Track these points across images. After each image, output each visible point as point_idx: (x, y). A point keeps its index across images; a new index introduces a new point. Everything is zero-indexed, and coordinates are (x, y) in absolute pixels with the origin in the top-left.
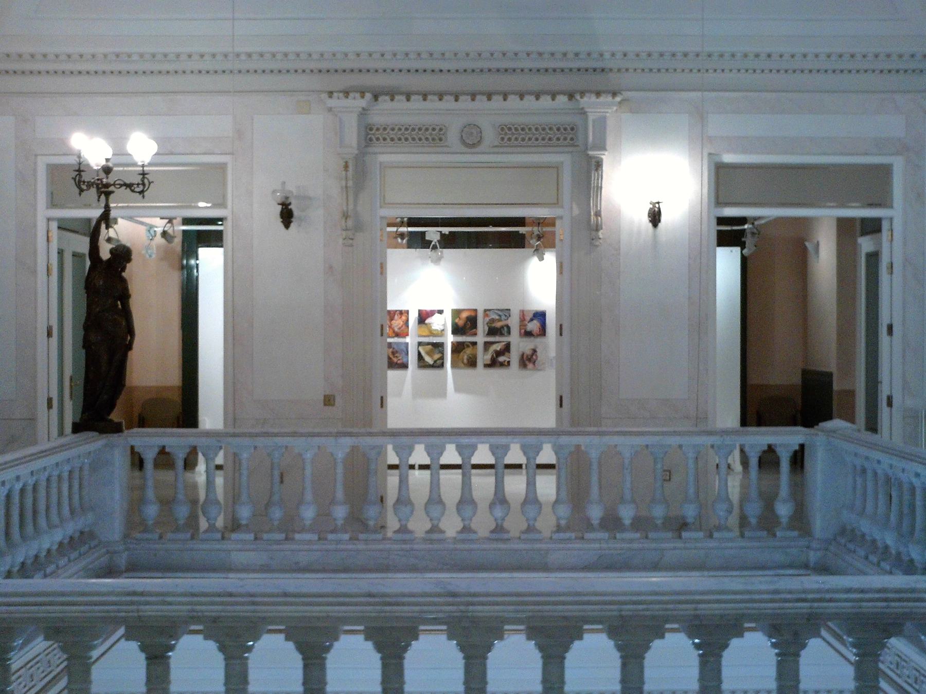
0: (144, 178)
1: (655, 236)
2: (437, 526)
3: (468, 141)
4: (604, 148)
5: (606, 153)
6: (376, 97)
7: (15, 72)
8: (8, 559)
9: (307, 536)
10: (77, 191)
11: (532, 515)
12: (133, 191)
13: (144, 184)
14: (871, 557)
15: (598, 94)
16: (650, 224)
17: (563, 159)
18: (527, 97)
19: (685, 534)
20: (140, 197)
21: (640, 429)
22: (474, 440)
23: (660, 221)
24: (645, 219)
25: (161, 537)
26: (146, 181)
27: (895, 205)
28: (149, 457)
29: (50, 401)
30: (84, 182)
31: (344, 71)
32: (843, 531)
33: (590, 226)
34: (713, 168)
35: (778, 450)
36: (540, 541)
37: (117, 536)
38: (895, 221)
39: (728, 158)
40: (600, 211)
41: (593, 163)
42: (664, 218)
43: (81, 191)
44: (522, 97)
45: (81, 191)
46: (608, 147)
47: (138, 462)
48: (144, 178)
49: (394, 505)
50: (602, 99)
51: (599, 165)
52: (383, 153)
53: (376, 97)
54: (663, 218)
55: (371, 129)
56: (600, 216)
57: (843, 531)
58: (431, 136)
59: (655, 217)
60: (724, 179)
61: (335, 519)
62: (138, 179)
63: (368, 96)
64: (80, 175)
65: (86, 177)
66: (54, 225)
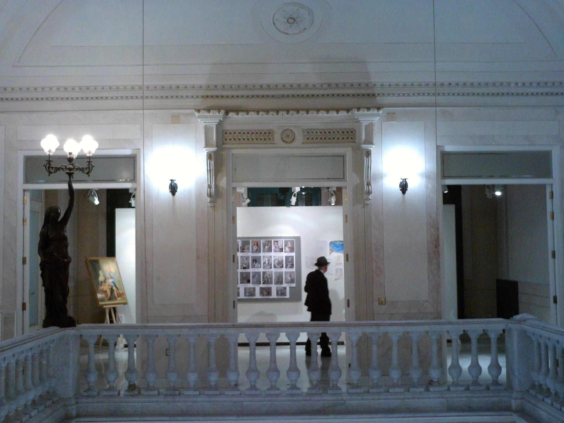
0: (89, 164)
1: (174, 201)
2: (254, 386)
3: (286, 140)
4: (371, 143)
5: (373, 146)
6: (227, 113)
7: (27, 99)
8: (6, 407)
9: (191, 392)
10: (48, 173)
11: (274, 378)
12: (83, 172)
13: (89, 168)
14: (555, 404)
15: (368, 109)
16: (171, 194)
17: (347, 151)
18: (261, 113)
19: (431, 389)
20: (86, 175)
21: (400, 322)
22: (296, 330)
23: (407, 190)
24: (397, 188)
25: (98, 394)
26: (90, 166)
27: (554, 175)
28: (92, 342)
29: (24, 305)
30: (52, 168)
31: (217, 97)
32: (533, 386)
33: (363, 191)
34: (439, 154)
35: (489, 333)
36: (300, 395)
37: (71, 394)
38: (554, 186)
39: (449, 148)
40: (370, 182)
41: (364, 153)
42: (179, 190)
43: (50, 173)
44: (258, 112)
45: (50, 173)
46: (374, 142)
47: (84, 345)
48: (89, 164)
49: (288, 371)
50: (371, 112)
51: (368, 154)
52: (233, 148)
53: (227, 113)
54: (178, 190)
55: (226, 133)
56: (370, 185)
57: (533, 386)
58: (265, 137)
59: (173, 189)
60: (446, 161)
61: (373, 380)
62: (86, 165)
63: (223, 112)
64: (49, 163)
65: (53, 165)
66: (28, 195)
